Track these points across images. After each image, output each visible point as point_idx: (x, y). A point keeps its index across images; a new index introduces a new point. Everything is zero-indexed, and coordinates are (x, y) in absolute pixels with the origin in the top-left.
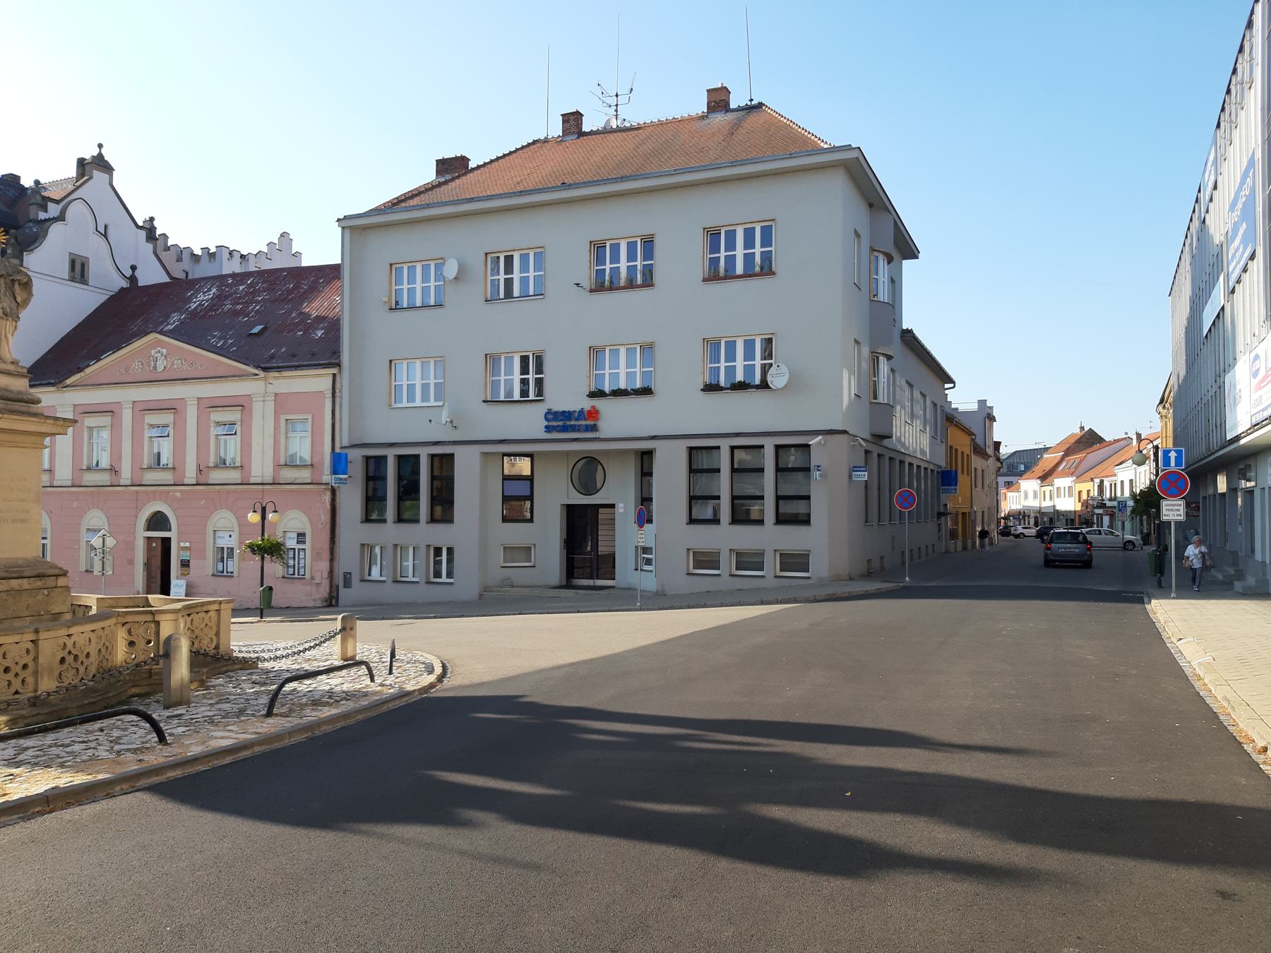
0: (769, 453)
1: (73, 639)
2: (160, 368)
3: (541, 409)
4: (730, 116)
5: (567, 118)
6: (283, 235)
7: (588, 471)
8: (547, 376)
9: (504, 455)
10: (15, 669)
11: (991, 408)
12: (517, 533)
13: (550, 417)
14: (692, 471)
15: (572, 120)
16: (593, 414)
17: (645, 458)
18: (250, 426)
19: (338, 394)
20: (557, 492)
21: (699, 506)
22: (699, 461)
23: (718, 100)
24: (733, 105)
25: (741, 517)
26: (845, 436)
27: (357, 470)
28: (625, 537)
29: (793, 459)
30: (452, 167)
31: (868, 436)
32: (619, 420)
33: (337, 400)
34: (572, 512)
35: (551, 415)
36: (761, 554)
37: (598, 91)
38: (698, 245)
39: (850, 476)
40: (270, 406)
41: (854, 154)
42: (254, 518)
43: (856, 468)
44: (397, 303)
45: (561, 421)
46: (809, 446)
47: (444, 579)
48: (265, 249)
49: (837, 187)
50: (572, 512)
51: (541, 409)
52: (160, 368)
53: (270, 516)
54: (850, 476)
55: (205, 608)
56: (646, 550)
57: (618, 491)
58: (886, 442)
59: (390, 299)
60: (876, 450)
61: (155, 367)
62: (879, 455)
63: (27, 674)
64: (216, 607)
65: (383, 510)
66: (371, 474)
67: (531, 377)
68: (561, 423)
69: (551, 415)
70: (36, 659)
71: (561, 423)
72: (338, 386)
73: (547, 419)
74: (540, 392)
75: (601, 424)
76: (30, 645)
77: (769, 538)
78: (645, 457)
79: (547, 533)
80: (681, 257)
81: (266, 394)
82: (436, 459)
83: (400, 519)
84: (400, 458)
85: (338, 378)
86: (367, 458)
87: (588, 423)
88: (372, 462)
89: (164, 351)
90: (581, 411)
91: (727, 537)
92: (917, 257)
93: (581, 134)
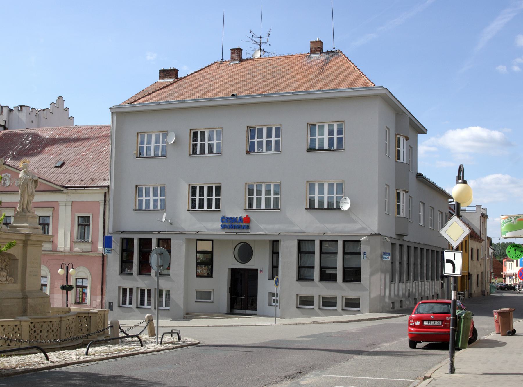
0: (340, 244)
1: (52, 323)
2: (7, 184)
3: (219, 216)
4: (323, 57)
5: (233, 51)
6: (60, 98)
7: (245, 251)
8: (222, 197)
9: (198, 240)
10: (55, 331)
11: (485, 210)
12: (204, 284)
13: (224, 220)
14: (300, 252)
15: (237, 52)
16: (247, 220)
17: (275, 244)
18: (58, 219)
19: (107, 203)
20: (225, 263)
21: (303, 274)
22: (304, 246)
23: (317, 47)
24: (324, 50)
25: (327, 276)
26: (380, 236)
27: (117, 246)
28: (265, 286)
29: (351, 249)
30: (169, 73)
31: (394, 236)
32: (264, 226)
33: (107, 207)
34: (234, 272)
35: (224, 219)
36: (335, 298)
37: (251, 35)
38: (304, 130)
39: (381, 258)
40: (69, 208)
41: (384, 92)
42: (61, 271)
43: (384, 254)
44: (140, 154)
45: (229, 223)
46: (360, 241)
47: (164, 307)
48: (49, 107)
49: (377, 107)
50: (234, 272)
51: (219, 216)
52: (7, 184)
53: (71, 271)
54: (381, 258)
55: (45, 320)
56: (274, 295)
57: (260, 262)
58: (405, 238)
59: (137, 152)
60: (398, 243)
61: (4, 184)
62: (400, 245)
63: (58, 333)
64: (103, 312)
65: (131, 268)
66: (124, 248)
67: (214, 197)
68: (230, 224)
69: (224, 219)
70: (60, 328)
71: (230, 224)
72: (107, 198)
73: (222, 221)
74: (218, 206)
75: (251, 225)
76: (59, 323)
77: (340, 290)
78: (275, 243)
79: (220, 285)
80: (294, 137)
81: (66, 202)
82: (161, 241)
83: (140, 273)
84: (141, 240)
85: (107, 195)
86: (123, 239)
87: (245, 224)
88: (125, 241)
89: (10, 175)
90: (241, 218)
91: (317, 289)
92: (425, 133)
93: (241, 60)
